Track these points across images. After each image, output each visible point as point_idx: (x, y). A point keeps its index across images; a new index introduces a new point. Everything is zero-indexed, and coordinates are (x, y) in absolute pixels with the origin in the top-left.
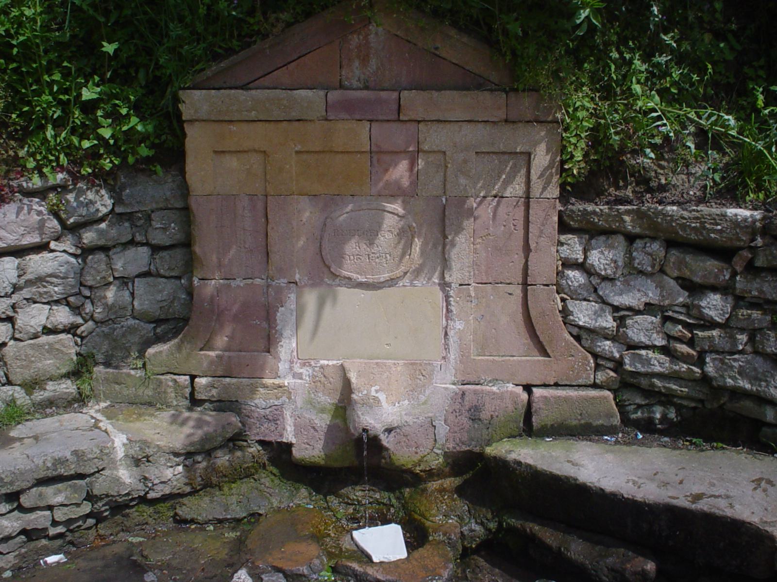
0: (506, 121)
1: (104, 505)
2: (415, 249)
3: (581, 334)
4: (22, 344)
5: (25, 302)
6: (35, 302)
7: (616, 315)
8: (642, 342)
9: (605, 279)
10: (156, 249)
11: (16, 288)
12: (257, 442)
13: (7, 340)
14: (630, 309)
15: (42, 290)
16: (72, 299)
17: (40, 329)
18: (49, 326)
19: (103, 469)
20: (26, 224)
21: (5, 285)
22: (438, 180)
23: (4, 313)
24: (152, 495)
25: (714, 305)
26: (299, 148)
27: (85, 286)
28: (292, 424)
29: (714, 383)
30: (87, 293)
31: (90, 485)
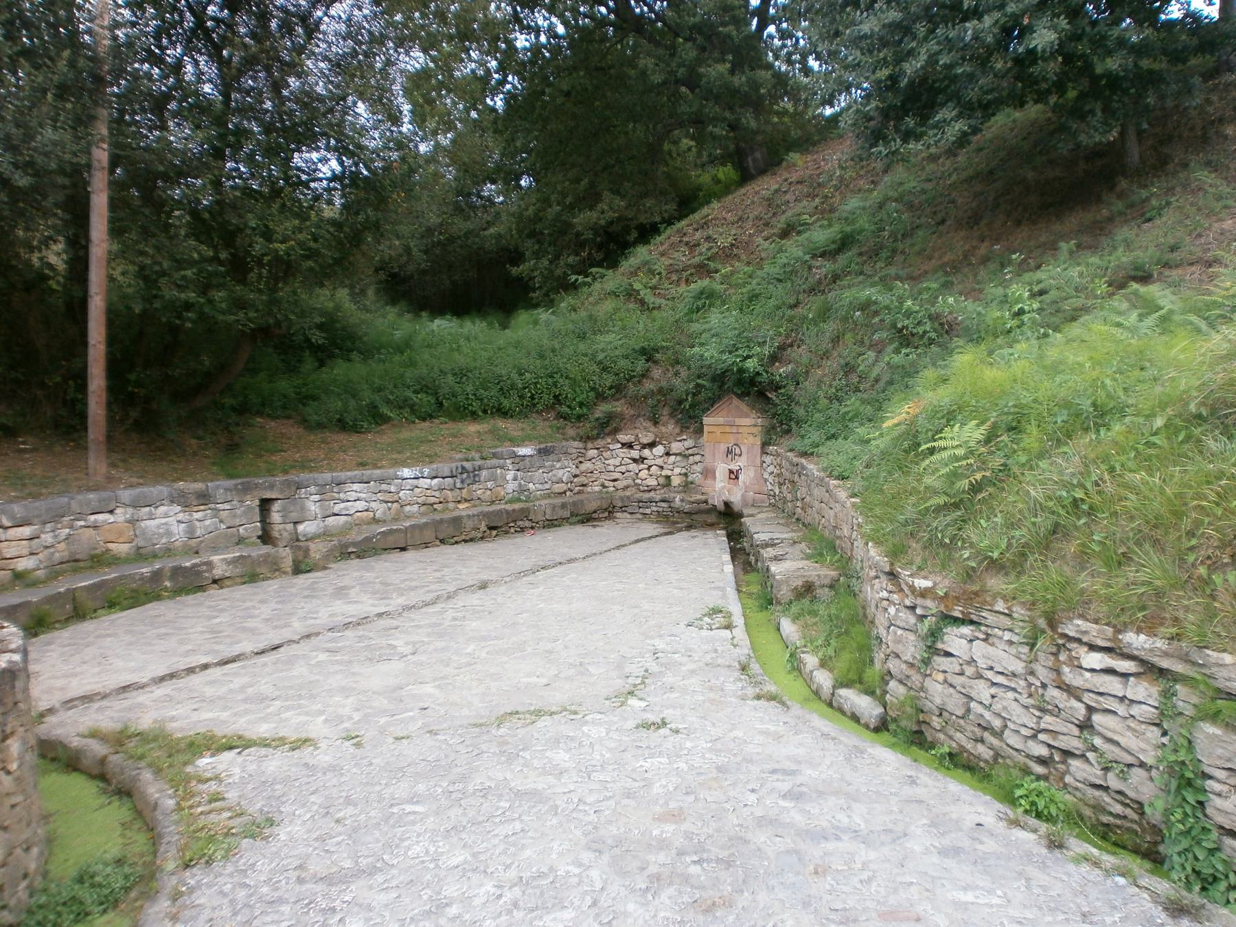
3: (766, 480)
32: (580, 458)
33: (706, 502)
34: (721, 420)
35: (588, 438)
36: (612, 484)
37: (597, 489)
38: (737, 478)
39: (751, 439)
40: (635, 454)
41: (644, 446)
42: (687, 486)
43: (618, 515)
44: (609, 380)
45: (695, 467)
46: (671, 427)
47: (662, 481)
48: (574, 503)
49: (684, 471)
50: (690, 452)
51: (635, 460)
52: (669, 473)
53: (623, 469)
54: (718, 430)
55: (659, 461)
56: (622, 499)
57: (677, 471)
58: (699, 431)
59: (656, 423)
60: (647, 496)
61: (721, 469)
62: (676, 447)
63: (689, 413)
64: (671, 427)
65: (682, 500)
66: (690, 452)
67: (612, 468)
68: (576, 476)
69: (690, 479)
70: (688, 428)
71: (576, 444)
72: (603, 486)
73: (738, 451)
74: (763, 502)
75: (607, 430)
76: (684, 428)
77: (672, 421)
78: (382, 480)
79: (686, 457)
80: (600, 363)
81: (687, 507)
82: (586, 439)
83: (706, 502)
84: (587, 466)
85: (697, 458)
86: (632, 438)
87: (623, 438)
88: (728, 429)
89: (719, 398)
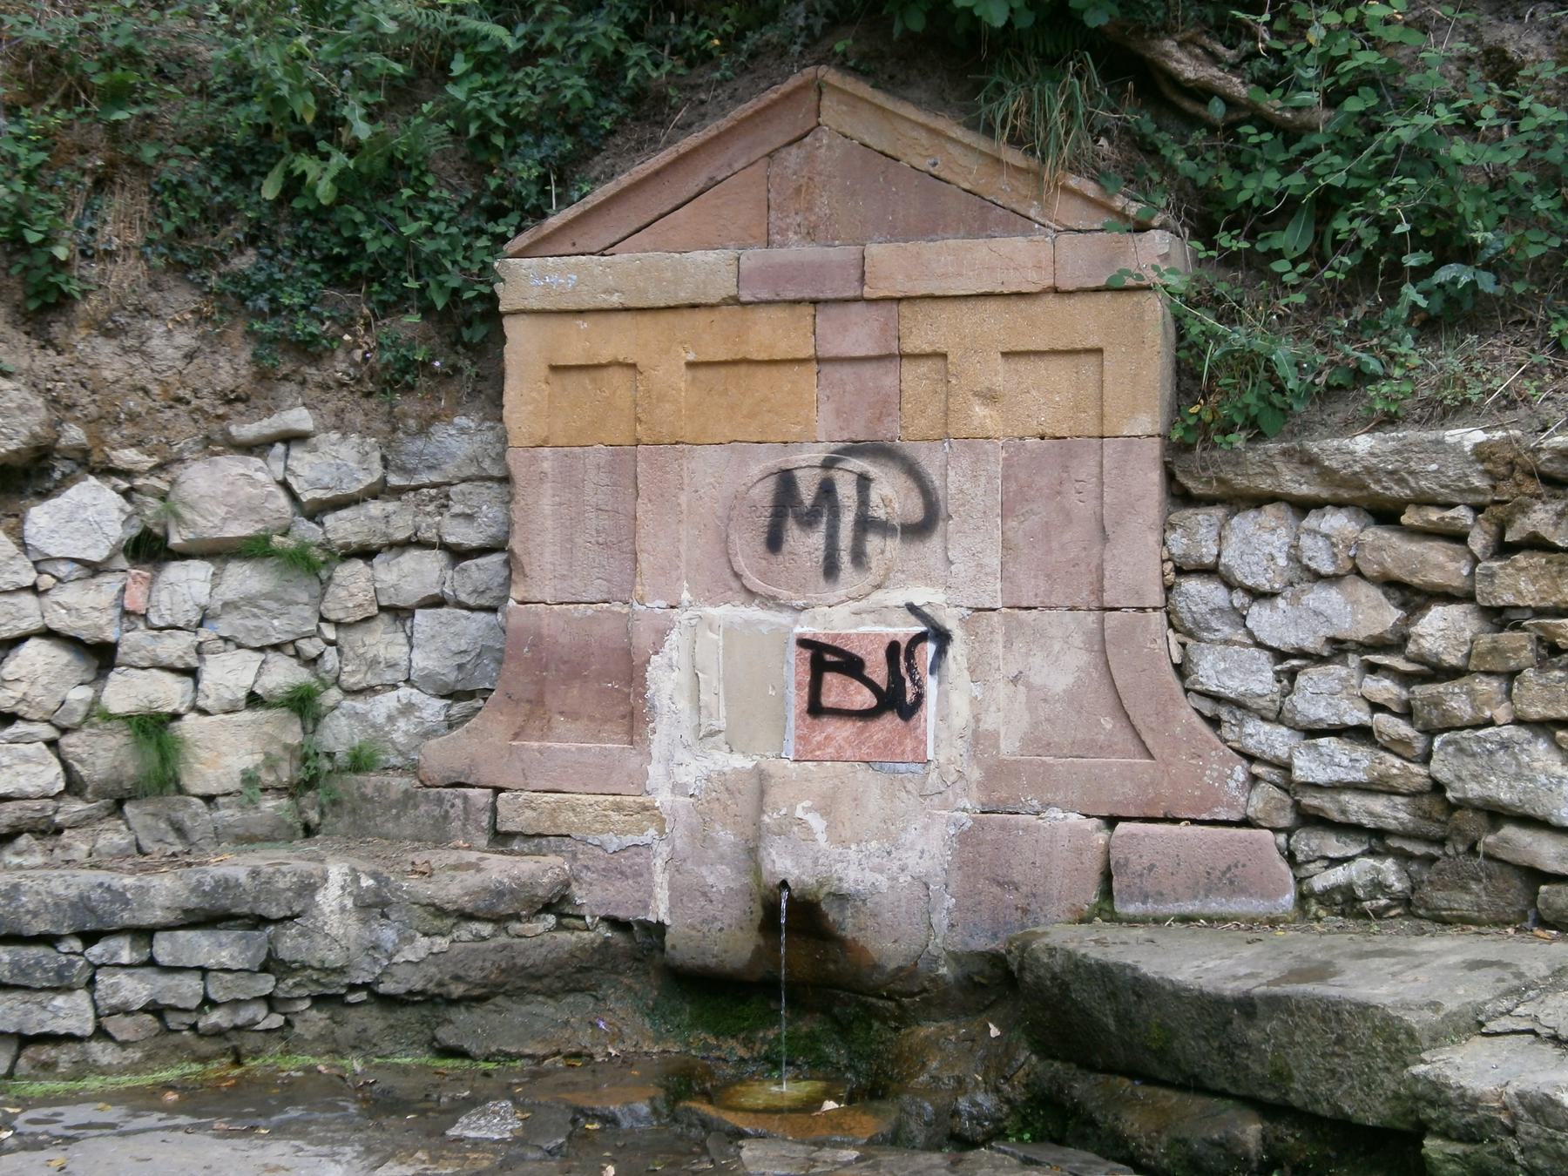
0: (1055, 290)
1: (296, 985)
3: (1219, 709)
4: (208, 719)
5: (220, 643)
6: (239, 646)
7: (1278, 668)
8: (1321, 720)
10: (458, 554)
11: (205, 617)
12: (603, 919)
13: (182, 710)
14: (1301, 654)
15: (251, 623)
16: (302, 644)
17: (242, 694)
18: (259, 691)
19: (298, 916)
20: (232, 501)
21: (187, 607)
22: (934, 410)
23: (181, 657)
24: (387, 987)
25: (1440, 630)
26: (691, 357)
27: (327, 621)
28: (666, 886)
29: (1449, 795)
30: (330, 633)
33: (557, 905)
34: (707, 268)
38: (896, 701)
39: (1048, 396)
42: (318, 790)
45: (383, 642)
46: (168, 343)
47: (103, 755)
49: (283, 675)
50: (344, 527)
52: (169, 693)
54: (666, 353)
55: (88, 608)
57: (229, 674)
58: (471, 335)
61: (715, 658)
62: (221, 492)
64: (168, 343)
65: (374, 906)
66: (344, 527)
69: (340, 732)
70: (309, 350)
73: (892, 495)
74: (1229, 880)
76: (290, 353)
77: (182, 298)
78: (200, 864)
79: (311, 566)
81: (413, 956)
85: (416, 574)
88: (773, 333)
89: (649, 111)
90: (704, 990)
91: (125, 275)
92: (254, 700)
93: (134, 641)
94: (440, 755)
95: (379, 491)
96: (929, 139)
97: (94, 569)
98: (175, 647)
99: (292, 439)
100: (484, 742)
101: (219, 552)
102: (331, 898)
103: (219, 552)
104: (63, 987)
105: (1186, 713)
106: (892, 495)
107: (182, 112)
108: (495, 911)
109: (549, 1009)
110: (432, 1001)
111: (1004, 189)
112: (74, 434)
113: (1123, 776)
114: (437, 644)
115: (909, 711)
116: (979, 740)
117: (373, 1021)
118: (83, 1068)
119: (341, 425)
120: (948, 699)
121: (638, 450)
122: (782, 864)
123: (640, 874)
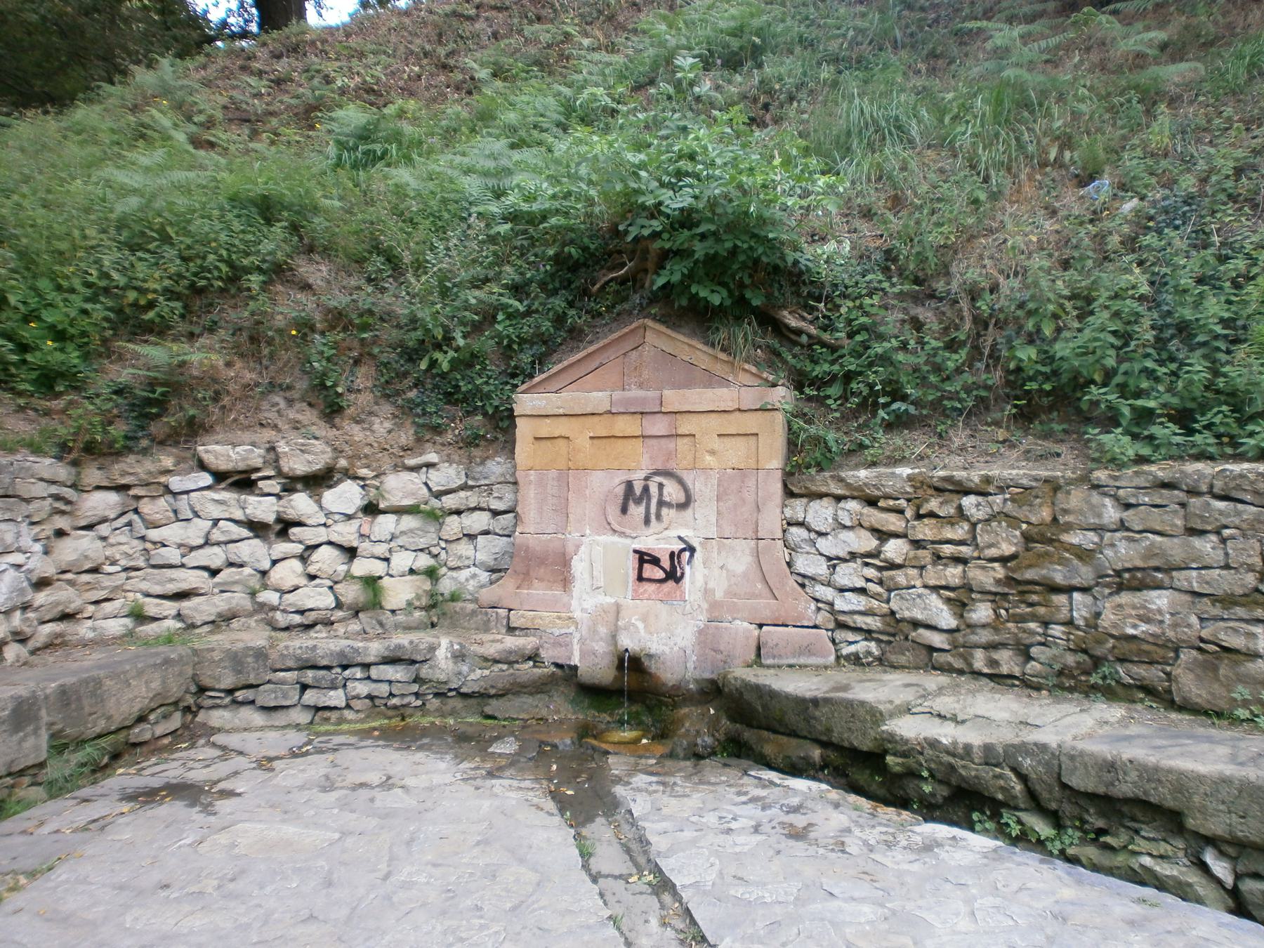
2: (941, 691)
3: (805, 581)
9: (820, 534)
10: (495, 513)
11: (393, 538)
14: (838, 558)
25: (895, 550)
30: (443, 545)
31: (418, 670)
32: (61, 519)
33: (534, 657)
34: (598, 399)
35: (90, 449)
36: (170, 607)
37: (116, 627)
38: (673, 576)
39: (736, 452)
40: (263, 508)
41: (292, 484)
42: (437, 609)
43: (217, 718)
44: (153, 277)
45: (464, 548)
46: (381, 426)
47: (351, 593)
48: (65, 697)
49: (424, 561)
50: (450, 502)
51: (257, 528)
52: (378, 568)
53: (214, 556)
54: (581, 433)
55: (346, 533)
56: (236, 660)
57: (403, 561)
59: (332, 411)
60: (298, 644)
62: (401, 487)
63: (461, 389)
64: (381, 426)
65: (459, 657)
66: (450, 502)
67: (172, 555)
68: (41, 584)
69: (446, 585)
70: (437, 430)
71: (46, 465)
72: (140, 617)
73: (672, 492)
74: (808, 650)
75: (156, 428)
77: (387, 408)
79: (435, 517)
80: (121, 225)
81: (475, 677)
82: (86, 450)
83: (534, 657)
84: (80, 547)
85: (479, 521)
86: (256, 457)
87: (222, 452)
88: (625, 425)
89: (576, 335)
90: (594, 693)
91: (365, 399)
92: (412, 571)
93: (364, 547)
94: (487, 595)
95: (465, 487)
96: (688, 347)
97: (349, 517)
98: (381, 549)
99: (430, 465)
100: (505, 590)
101: (399, 511)
102: (442, 654)
103: (399, 511)
104: (333, 687)
105: (791, 582)
106: (672, 492)
107: (389, 334)
108: (509, 659)
109: (530, 700)
110: (482, 696)
111: (718, 369)
112: (343, 463)
113: (766, 607)
114: (487, 550)
115: (678, 580)
116: (707, 592)
117: (458, 704)
118: (341, 721)
119: (450, 461)
120: (694, 574)
121: (569, 472)
122: (627, 642)
123: (568, 645)
